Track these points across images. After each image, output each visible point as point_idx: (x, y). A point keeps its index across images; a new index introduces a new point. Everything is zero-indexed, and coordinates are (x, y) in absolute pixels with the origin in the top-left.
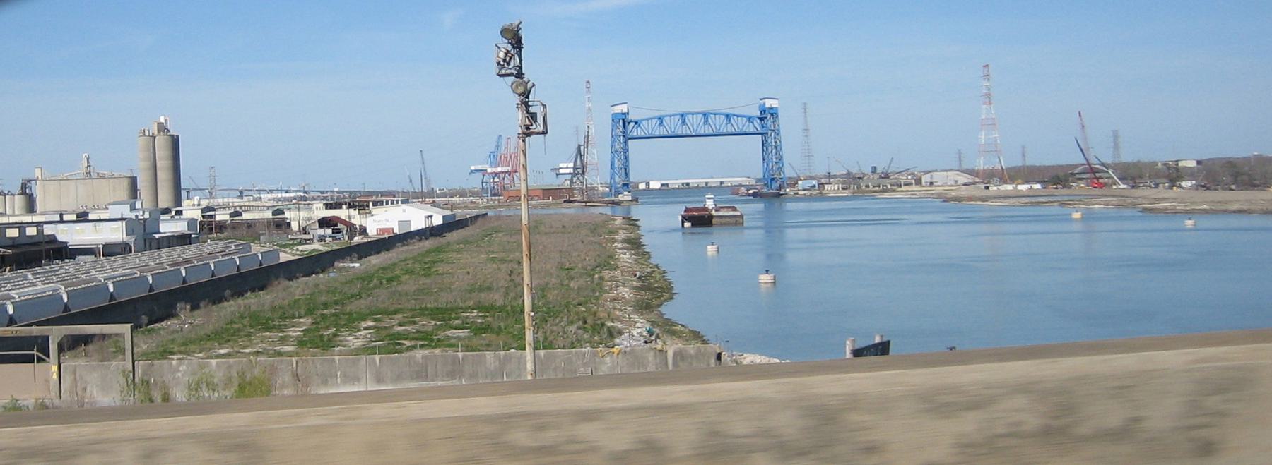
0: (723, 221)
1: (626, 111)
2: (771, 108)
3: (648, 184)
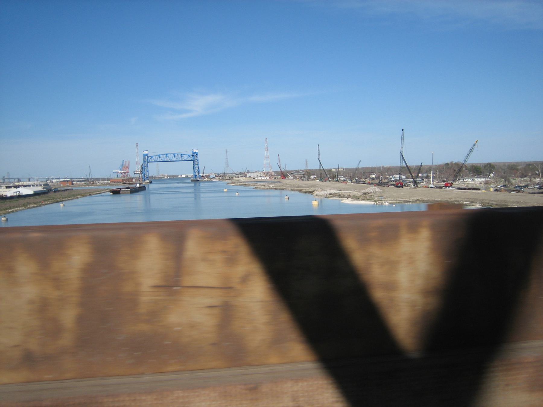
0: (124, 192)
1: (147, 153)
2: (196, 152)
3: (181, 176)
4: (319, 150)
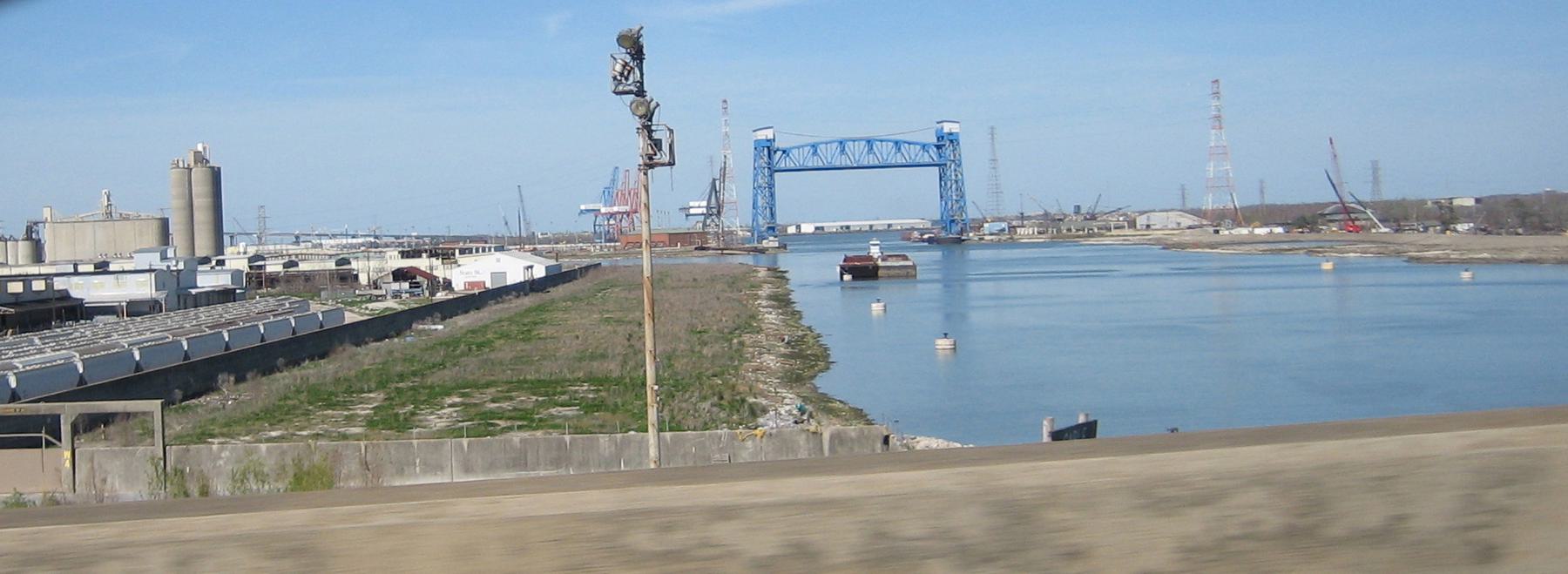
0: (892, 272)
1: (772, 137)
2: (951, 134)
3: (798, 227)
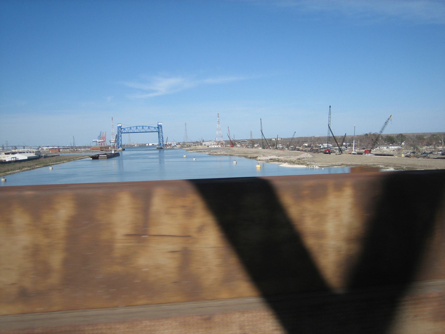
0: (101, 158)
1: (121, 126)
2: (160, 125)
3: (148, 144)
4: (261, 123)
